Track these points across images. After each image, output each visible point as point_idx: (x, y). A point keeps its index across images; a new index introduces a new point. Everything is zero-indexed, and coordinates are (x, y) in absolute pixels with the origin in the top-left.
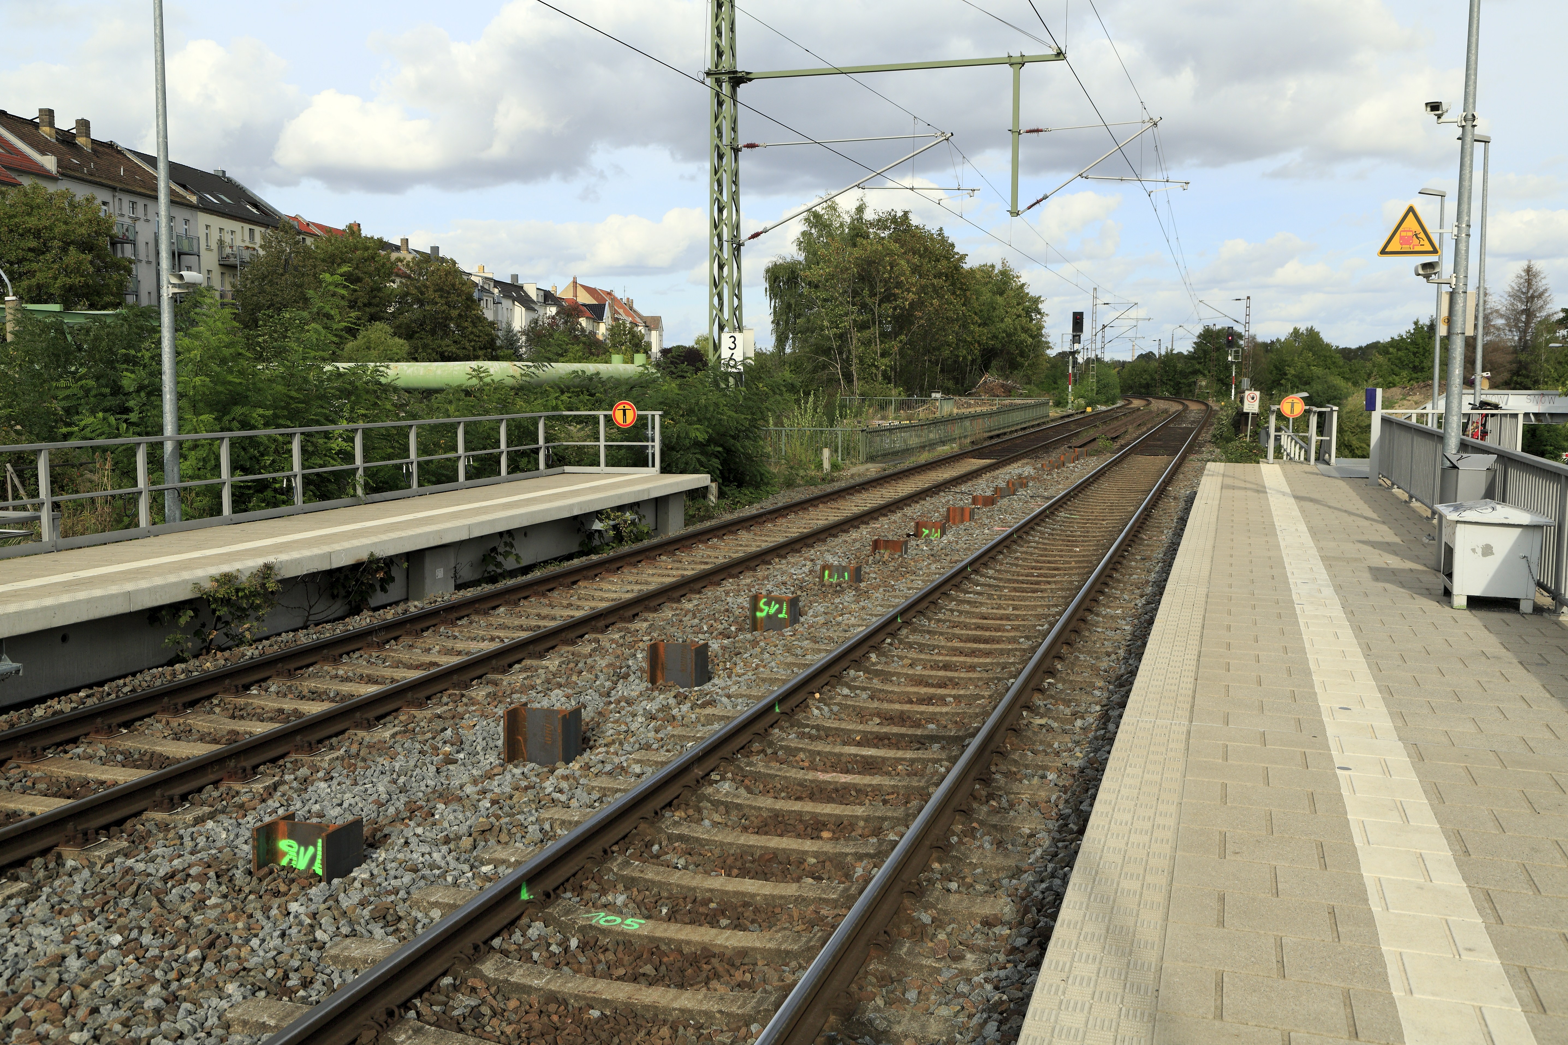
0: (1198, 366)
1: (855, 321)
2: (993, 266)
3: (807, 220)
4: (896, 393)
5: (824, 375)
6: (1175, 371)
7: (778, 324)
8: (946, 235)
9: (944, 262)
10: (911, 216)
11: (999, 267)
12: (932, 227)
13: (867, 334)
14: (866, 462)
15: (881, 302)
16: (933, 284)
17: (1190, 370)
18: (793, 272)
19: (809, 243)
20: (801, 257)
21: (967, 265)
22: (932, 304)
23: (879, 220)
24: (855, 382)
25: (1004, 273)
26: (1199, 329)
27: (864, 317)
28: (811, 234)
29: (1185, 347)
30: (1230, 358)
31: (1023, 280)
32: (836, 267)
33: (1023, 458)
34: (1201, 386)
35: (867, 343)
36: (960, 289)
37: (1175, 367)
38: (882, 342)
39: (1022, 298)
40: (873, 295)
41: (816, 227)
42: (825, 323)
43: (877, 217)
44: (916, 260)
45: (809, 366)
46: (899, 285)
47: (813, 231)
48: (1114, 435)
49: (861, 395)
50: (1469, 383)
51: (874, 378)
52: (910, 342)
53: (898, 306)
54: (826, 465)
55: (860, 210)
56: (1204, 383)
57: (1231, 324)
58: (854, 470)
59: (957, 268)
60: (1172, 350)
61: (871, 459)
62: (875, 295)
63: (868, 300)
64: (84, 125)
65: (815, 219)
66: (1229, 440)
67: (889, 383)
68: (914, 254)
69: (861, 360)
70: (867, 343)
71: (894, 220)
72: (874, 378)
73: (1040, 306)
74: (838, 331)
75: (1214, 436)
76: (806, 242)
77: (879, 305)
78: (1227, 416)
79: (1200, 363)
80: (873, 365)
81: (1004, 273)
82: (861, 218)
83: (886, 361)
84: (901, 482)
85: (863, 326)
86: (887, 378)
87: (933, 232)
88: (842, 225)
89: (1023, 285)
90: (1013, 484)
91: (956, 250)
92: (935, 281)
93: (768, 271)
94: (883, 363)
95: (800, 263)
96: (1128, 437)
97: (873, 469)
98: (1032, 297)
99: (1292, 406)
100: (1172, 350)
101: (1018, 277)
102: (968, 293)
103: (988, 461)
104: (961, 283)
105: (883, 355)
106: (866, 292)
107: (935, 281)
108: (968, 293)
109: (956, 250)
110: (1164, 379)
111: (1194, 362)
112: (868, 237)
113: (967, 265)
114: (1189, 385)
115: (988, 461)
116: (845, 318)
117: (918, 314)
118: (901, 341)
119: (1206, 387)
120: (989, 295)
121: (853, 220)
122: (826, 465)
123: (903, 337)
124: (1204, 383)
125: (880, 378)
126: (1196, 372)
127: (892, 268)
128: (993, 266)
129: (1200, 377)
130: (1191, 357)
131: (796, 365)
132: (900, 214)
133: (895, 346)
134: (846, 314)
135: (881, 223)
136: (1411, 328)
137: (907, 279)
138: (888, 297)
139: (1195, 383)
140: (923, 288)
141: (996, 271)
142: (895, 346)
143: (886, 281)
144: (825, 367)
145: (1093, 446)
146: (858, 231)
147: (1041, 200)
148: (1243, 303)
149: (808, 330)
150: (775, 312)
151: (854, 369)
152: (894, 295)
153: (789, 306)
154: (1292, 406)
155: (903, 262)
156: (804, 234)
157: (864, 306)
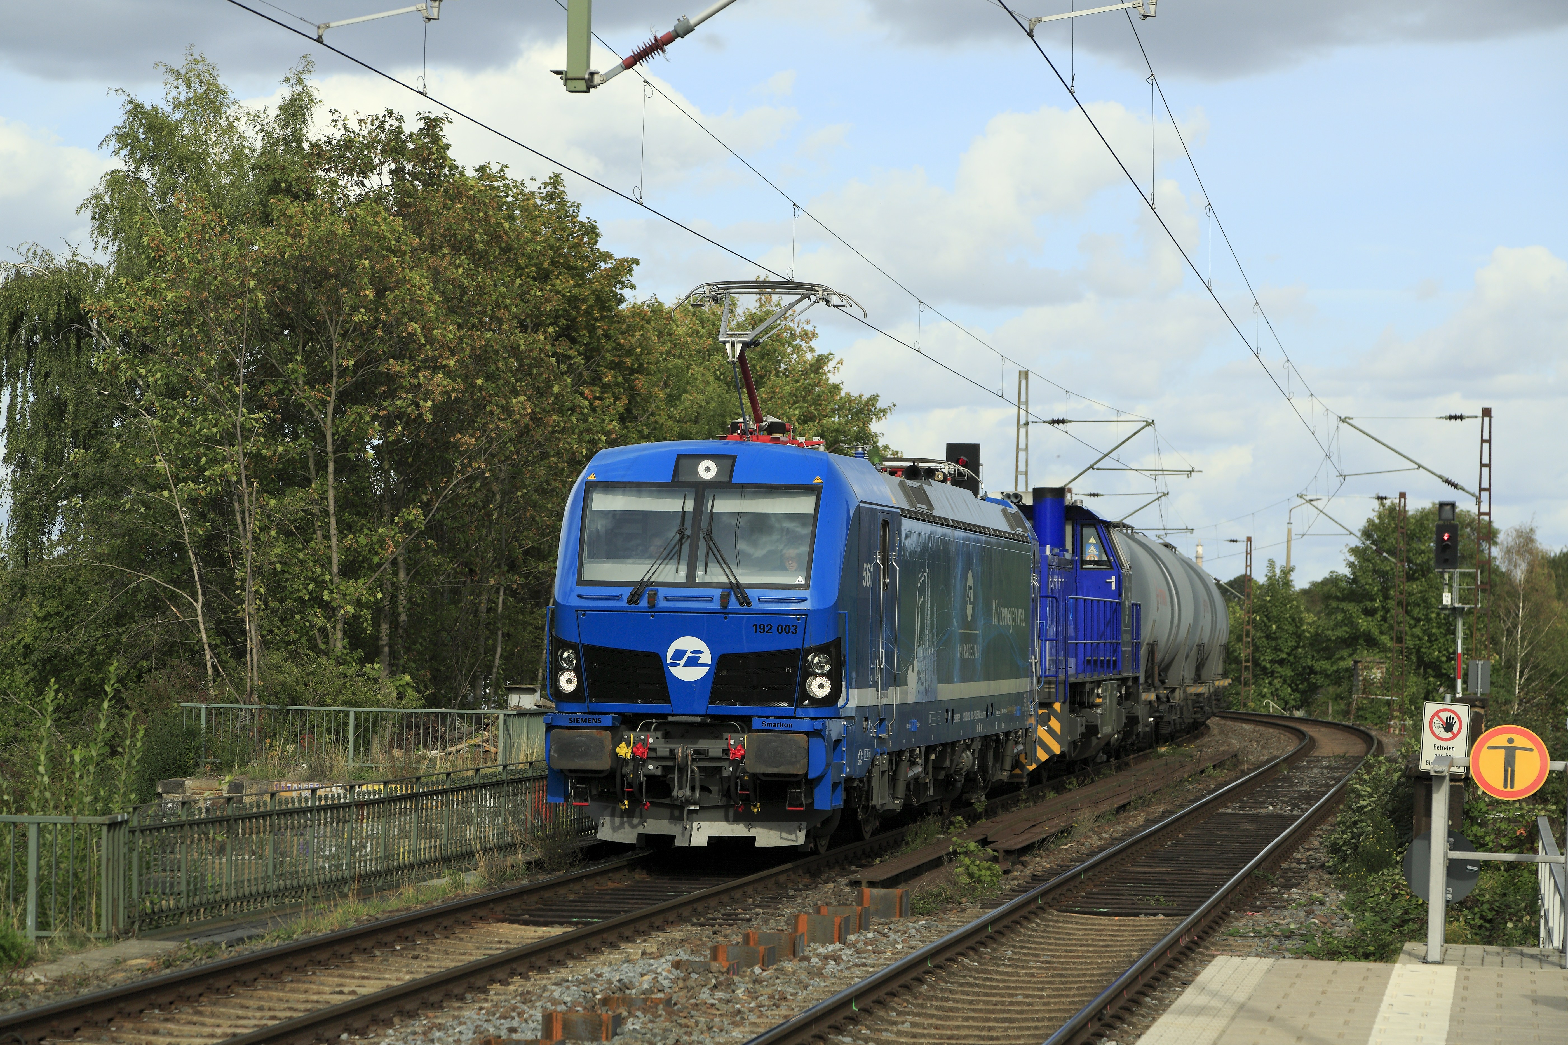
0: (1363, 623)
1: (255, 458)
3: (125, 138)
4: (392, 692)
5: (153, 631)
6: (1299, 636)
7: (24, 464)
8: (571, 196)
9: (564, 283)
10: (448, 133)
12: (527, 173)
13: (294, 502)
14: (125, 934)
15: (345, 398)
16: (514, 350)
17: (1343, 632)
18: (73, 301)
19: (127, 210)
20: (100, 254)
21: (636, 295)
22: (507, 410)
23: (348, 144)
24: (253, 656)
26: (1361, 512)
29: (1321, 558)
30: (1447, 599)
31: (820, 347)
32: (200, 284)
33: (682, 920)
34: (1368, 683)
35: (300, 530)
36: (615, 366)
37: (1297, 622)
38: (345, 528)
39: (817, 401)
40: (319, 376)
41: (153, 159)
42: (161, 464)
44: (458, 269)
45: (101, 601)
46: (404, 348)
47: (145, 173)
49: (268, 695)
50: (179, 861)
51: (317, 644)
52: (434, 529)
53: (400, 415)
55: (295, 110)
56: (1377, 674)
57: (1448, 494)
58: (71, 963)
59: (606, 302)
60: (1287, 571)
61: (149, 923)
63: (305, 395)
65: (147, 135)
66: (1376, 863)
67: (370, 658)
68: (456, 249)
69: (276, 584)
70: (300, 530)
71: (395, 146)
72: (317, 644)
73: (875, 427)
74: (204, 491)
75: (1335, 849)
76: (116, 211)
78: (1376, 783)
79: (1369, 613)
80: (316, 600)
83: (358, 588)
84: (186, 1013)
85: (283, 477)
86: (362, 645)
87: (531, 187)
88: (237, 157)
89: (821, 361)
90: (567, 1026)
91: (602, 245)
92: (522, 340)
94: (350, 596)
95: (98, 271)
98: (849, 399)
99: (1510, 762)
101: (806, 336)
102: (641, 382)
103: (555, 931)
104: (619, 347)
105: (350, 570)
106: (297, 368)
107: (522, 340)
108: (641, 382)
109: (602, 245)
110: (1265, 660)
111: (1352, 608)
112: (310, 196)
113: (636, 295)
114: (1337, 678)
115: (555, 931)
116: (224, 450)
117: (467, 441)
118: (408, 527)
119: (1385, 686)
120: (714, 388)
121: (271, 143)
123: (414, 513)
124: (1377, 674)
125: (339, 642)
126: (1358, 640)
127: (380, 294)
129: (1365, 655)
130: (1327, 593)
132: (412, 126)
133: (388, 539)
134: (228, 438)
135: (351, 155)
136: (619, 253)
137: (427, 330)
138: (366, 387)
139: (1351, 673)
140: (481, 358)
142: (388, 539)
143: (364, 334)
144: (155, 605)
145: (928, 883)
147: (670, 39)
148: (1472, 427)
149: (99, 482)
151: (249, 611)
152: (390, 378)
153: (58, 408)
154: (1510, 762)
155: (416, 277)
156: (115, 181)
157: (290, 414)
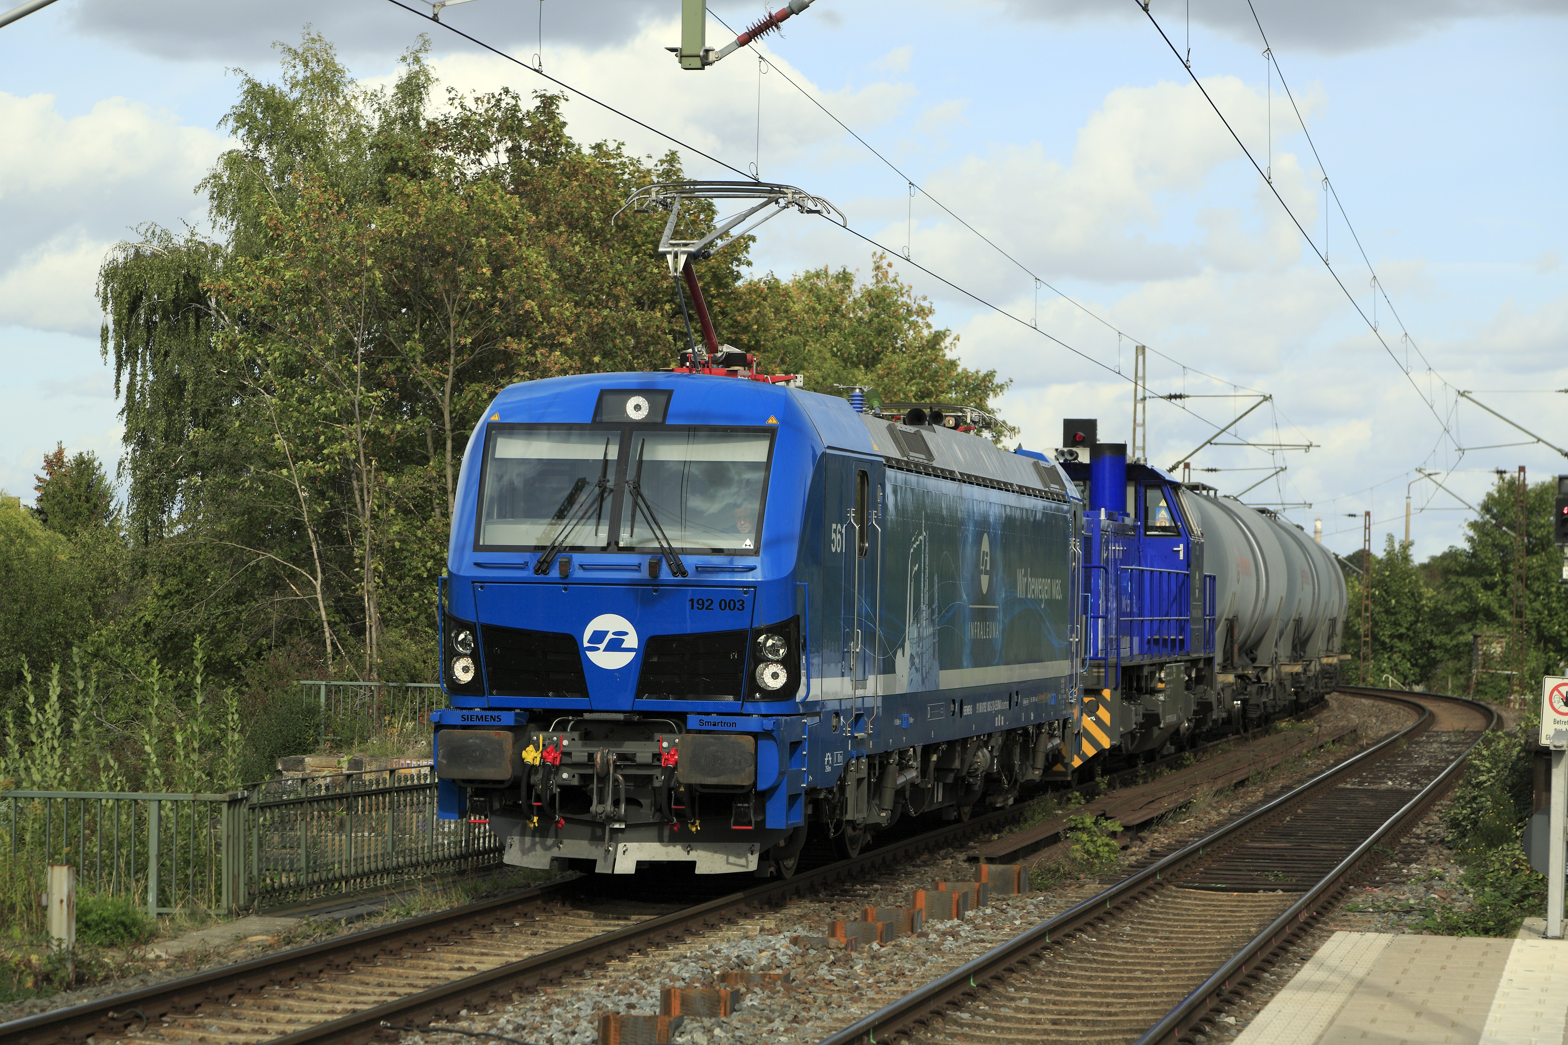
0: (1483, 598)
1: (374, 436)
2: (845, 278)
3: (243, 118)
5: (272, 609)
7: (143, 443)
10: (564, 111)
11: (864, 280)
14: (244, 911)
15: (463, 377)
17: (1462, 606)
18: (191, 280)
19: (245, 189)
20: (219, 234)
23: (465, 123)
24: (373, 634)
25: (879, 299)
26: (1480, 486)
27: (404, 425)
28: (258, 162)
29: (1440, 532)
32: (318, 263)
34: (1488, 658)
37: (1415, 596)
40: (436, 354)
41: (271, 140)
42: (280, 443)
43: (455, 112)
44: (575, 247)
45: (220, 579)
46: (521, 326)
48: (1136, 818)
49: (387, 672)
54: (60, 925)
55: (412, 89)
56: (1497, 649)
58: (192, 940)
60: (1406, 546)
61: (267, 899)
62: (445, 355)
63: (422, 373)
64: (808, 272)
65: (265, 114)
66: (1495, 838)
69: (395, 562)
71: (511, 124)
74: (323, 469)
75: (1455, 824)
76: (235, 188)
77: (457, 388)
78: (1495, 758)
79: (1489, 587)
81: (879, 299)
82: (414, 116)
88: (355, 135)
90: (685, 1002)
92: (638, 318)
93: (111, 274)
95: (216, 251)
96: (1187, 824)
97: (259, 934)
98: (966, 375)
100: (1406, 546)
101: (922, 312)
106: (414, 346)
107: (638, 318)
110: (1385, 635)
111: (1470, 581)
112: (427, 174)
114: (1456, 653)
116: (342, 429)
119: (1505, 660)
121: (388, 123)
122: (60, 925)
124: (1497, 649)
128: (845, 278)
129: (1486, 630)
131: (185, 575)
132: (528, 104)
134: (347, 416)
135: (469, 133)
139: (1471, 648)
141: (857, 290)
143: (481, 312)
146: (405, 151)
147: (784, 16)
149: (218, 461)
150: (131, 408)
151: (368, 589)
152: (507, 356)
153: (177, 386)
155: (533, 255)
156: (233, 161)
157: (409, 392)
